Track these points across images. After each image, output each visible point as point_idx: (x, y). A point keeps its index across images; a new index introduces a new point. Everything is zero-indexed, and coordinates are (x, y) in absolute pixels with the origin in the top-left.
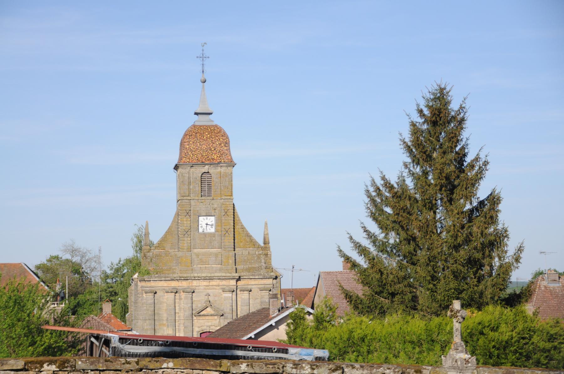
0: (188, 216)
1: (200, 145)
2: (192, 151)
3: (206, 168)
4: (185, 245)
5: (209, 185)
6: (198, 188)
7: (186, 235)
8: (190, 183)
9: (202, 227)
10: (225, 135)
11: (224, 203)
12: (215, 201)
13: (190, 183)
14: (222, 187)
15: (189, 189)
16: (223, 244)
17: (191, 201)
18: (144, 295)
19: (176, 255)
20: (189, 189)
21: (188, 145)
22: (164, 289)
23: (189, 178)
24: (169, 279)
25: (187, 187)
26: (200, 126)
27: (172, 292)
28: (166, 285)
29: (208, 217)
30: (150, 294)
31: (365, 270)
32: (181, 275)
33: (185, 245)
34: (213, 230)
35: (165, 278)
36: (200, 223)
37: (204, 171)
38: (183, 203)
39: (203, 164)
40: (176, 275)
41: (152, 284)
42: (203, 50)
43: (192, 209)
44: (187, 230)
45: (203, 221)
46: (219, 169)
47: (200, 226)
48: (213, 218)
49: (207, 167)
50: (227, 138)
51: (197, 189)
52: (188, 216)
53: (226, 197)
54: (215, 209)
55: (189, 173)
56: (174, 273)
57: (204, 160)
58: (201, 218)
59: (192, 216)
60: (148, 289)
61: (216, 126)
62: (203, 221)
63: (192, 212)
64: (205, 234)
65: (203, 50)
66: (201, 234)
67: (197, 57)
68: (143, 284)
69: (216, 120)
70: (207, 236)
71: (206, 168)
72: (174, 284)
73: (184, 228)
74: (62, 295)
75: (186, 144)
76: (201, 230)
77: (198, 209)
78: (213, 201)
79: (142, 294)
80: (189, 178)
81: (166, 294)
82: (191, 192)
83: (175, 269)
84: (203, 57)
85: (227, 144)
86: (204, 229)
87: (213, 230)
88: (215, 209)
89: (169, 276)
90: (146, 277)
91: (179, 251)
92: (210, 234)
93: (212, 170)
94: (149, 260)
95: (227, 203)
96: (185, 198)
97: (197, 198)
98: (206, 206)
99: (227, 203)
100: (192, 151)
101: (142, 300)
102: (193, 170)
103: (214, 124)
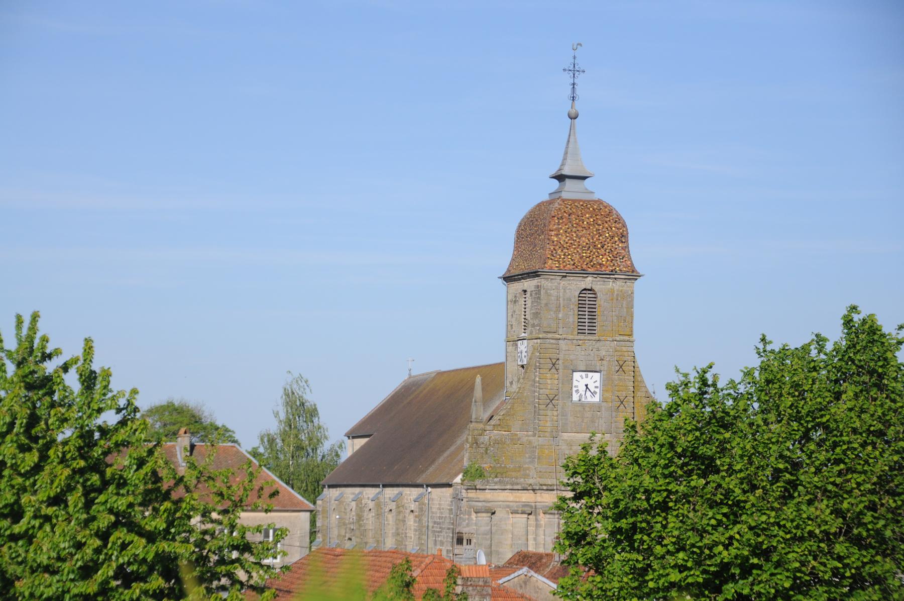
0: (553, 370)
3: (588, 282)
4: (549, 424)
5: (592, 315)
9: (577, 391)
10: (618, 220)
11: (618, 348)
12: (601, 343)
16: (613, 425)
17: (560, 342)
18: (474, 516)
19: (530, 442)
21: (557, 235)
22: (508, 507)
24: (519, 487)
26: (574, 201)
27: (523, 513)
28: (511, 499)
29: (590, 374)
30: (484, 515)
32: (542, 481)
33: (549, 424)
34: (597, 399)
35: (512, 485)
36: (575, 383)
37: (584, 287)
38: (547, 346)
39: (584, 273)
40: (531, 481)
41: (488, 495)
42: (575, 58)
44: (551, 397)
45: (580, 380)
46: (610, 284)
47: (574, 389)
48: (597, 376)
49: (590, 279)
50: (624, 226)
51: (571, 320)
52: (553, 370)
53: (622, 338)
56: (526, 476)
57: (584, 267)
58: (576, 375)
59: (561, 371)
60: (480, 504)
61: (599, 202)
62: (580, 380)
64: (582, 405)
65: (575, 58)
66: (575, 404)
67: (564, 70)
68: (472, 494)
69: (598, 189)
70: (587, 409)
71: (588, 282)
72: (527, 497)
73: (547, 392)
75: (553, 233)
76: (575, 398)
77: (572, 357)
78: (598, 344)
79: (470, 515)
80: (558, 299)
81: (511, 516)
83: (528, 469)
84: (574, 71)
85: (623, 237)
86: (581, 396)
87: (597, 399)
89: (518, 481)
90: (478, 483)
91: (534, 435)
92: (592, 405)
93: (601, 286)
94: (482, 450)
95: (624, 349)
96: (550, 335)
97: (571, 337)
101: (468, 525)
102: (564, 283)
103: (596, 197)
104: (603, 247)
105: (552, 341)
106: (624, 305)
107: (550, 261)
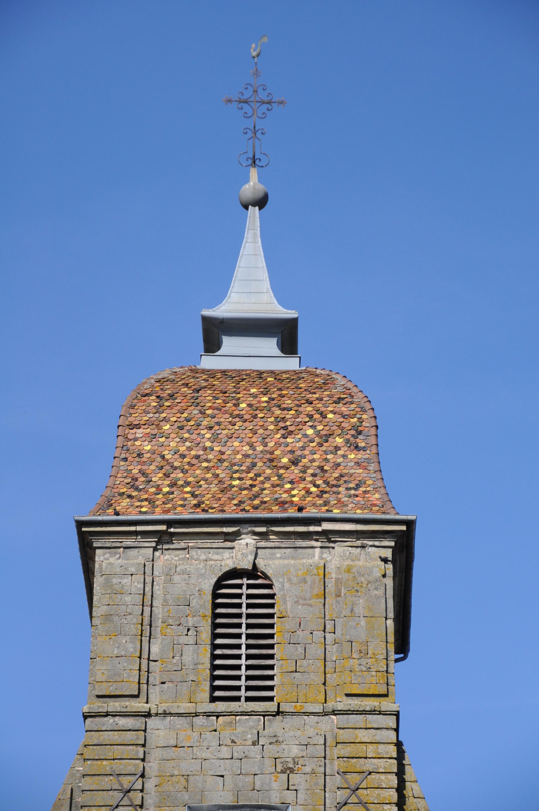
1: (215, 438)
2: (167, 468)
3: (243, 551)
6: (197, 656)
7: (263, 95)
8: (147, 630)
13: (147, 630)
14: (332, 650)
15: (145, 658)
17: (152, 722)
20: (145, 658)
23: (147, 600)
25: (132, 648)
31: (239, 406)
39: (227, 529)
43: (152, 767)
54: (288, 771)
55: (146, 571)
63: (150, 785)
67: (230, 101)
71: (243, 551)
74: (137, 459)
75: (139, 433)
77: (188, 766)
78: (276, 725)
80: (147, 600)
82: (155, 678)
88: (288, 771)
93: (279, 562)
95: (363, 736)
96: (114, 705)
98: (238, 751)
99: (363, 736)
100: (167, 468)
102: (166, 558)
104: (295, 462)
105: (123, 722)
106: (360, 610)
107: (126, 502)
